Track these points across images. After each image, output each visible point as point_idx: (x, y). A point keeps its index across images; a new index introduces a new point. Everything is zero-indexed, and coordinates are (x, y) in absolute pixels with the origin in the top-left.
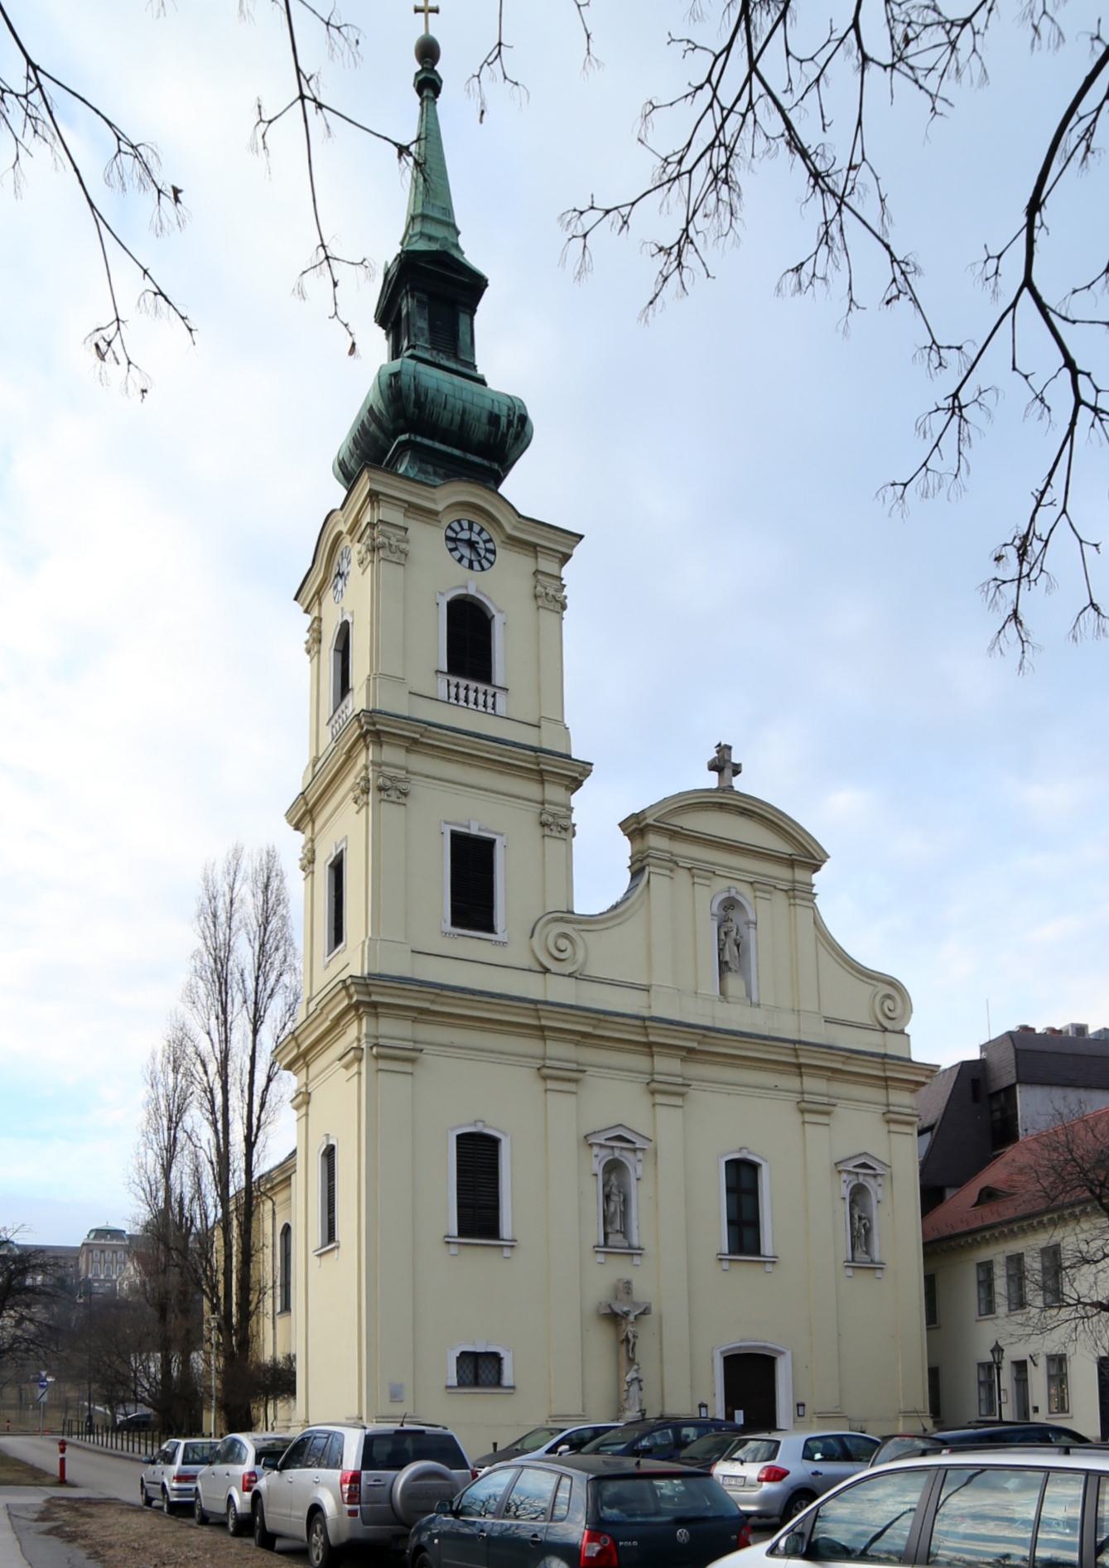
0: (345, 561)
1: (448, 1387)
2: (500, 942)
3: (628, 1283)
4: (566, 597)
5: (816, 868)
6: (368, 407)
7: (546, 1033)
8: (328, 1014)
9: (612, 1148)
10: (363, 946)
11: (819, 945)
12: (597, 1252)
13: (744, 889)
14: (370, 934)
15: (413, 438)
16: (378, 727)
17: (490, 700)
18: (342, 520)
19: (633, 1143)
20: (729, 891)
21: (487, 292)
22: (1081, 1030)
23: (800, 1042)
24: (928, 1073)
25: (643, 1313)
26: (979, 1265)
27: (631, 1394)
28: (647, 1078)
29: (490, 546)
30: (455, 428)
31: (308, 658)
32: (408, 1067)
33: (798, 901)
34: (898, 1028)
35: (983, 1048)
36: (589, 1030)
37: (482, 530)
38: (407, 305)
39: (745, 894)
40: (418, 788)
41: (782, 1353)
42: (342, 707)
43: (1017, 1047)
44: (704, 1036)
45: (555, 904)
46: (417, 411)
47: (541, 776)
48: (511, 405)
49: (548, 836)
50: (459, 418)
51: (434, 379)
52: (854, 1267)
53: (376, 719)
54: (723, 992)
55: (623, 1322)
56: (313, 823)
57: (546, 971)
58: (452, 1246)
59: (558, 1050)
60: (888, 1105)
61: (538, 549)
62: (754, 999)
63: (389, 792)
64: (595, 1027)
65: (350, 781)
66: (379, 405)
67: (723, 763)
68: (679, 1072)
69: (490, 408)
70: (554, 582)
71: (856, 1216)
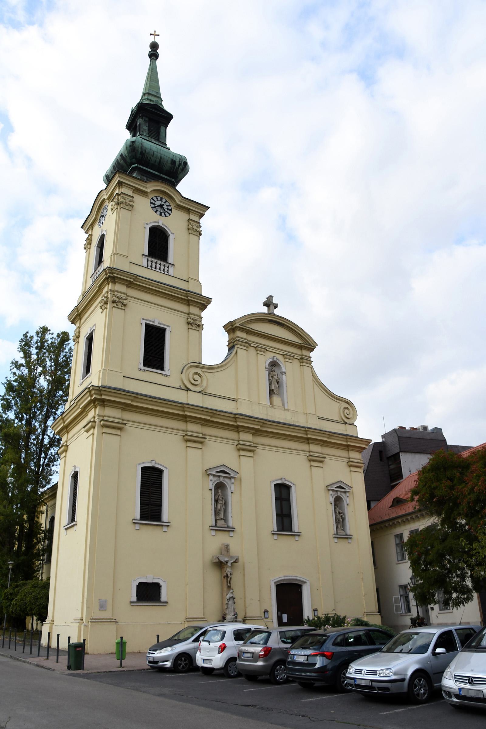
0: (105, 211)
1: (131, 602)
2: (166, 375)
3: (227, 546)
4: (201, 231)
5: (312, 350)
6: (121, 154)
7: (187, 419)
8: (80, 405)
9: (219, 476)
10: (100, 373)
11: (314, 384)
12: (211, 529)
13: (280, 357)
14: (103, 367)
15: (138, 166)
16: (114, 275)
17: (166, 269)
18: (105, 194)
19: (230, 474)
20: (273, 358)
21: (172, 121)
22: (425, 428)
23: (308, 428)
24: (366, 443)
25: (235, 562)
26: (396, 536)
27: (229, 606)
28: (236, 443)
29: (169, 208)
30: (156, 164)
31: (85, 251)
32: (118, 432)
33: (304, 364)
34: (351, 423)
35: (383, 437)
36: (209, 418)
37: (166, 201)
38: (139, 121)
39: (281, 360)
40: (131, 303)
41: (305, 582)
42: (99, 269)
43: (399, 435)
44: (263, 423)
45: (193, 359)
46: (141, 156)
47: (188, 303)
48: (181, 158)
49: (191, 328)
50: (159, 160)
51: (150, 145)
52: (337, 538)
53: (113, 271)
54: (271, 403)
55: (225, 566)
56: (81, 320)
57: (188, 389)
58: (136, 525)
59: (193, 428)
60: (349, 458)
61: (190, 211)
62: (286, 408)
63: (117, 304)
64: (211, 417)
65: (100, 299)
66: (125, 153)
67: (269, 303)
68: (251, 440)
69: (172, 158)
70: (197, 224)
71: (337, 512)
